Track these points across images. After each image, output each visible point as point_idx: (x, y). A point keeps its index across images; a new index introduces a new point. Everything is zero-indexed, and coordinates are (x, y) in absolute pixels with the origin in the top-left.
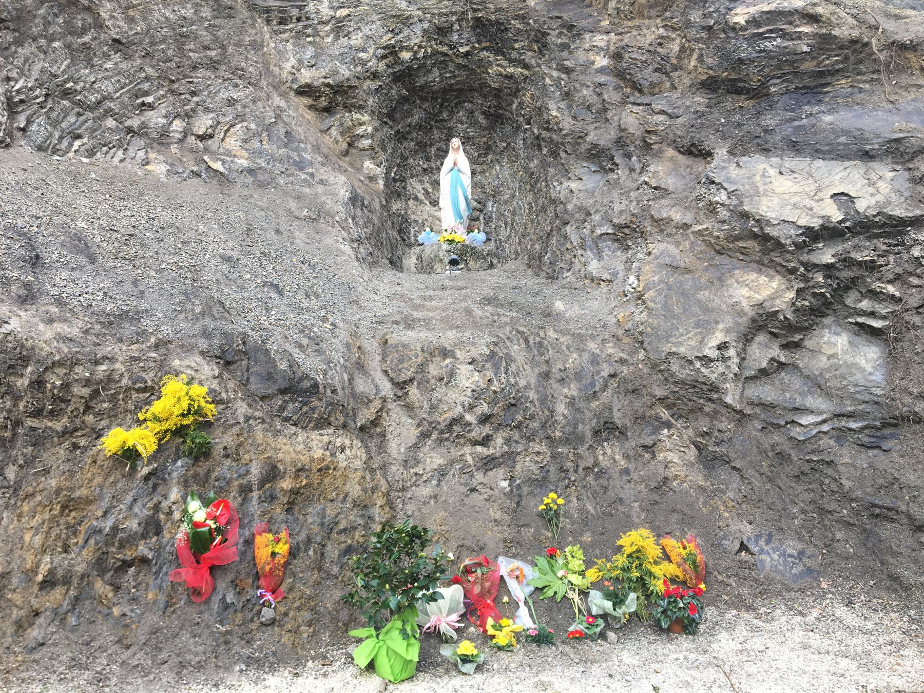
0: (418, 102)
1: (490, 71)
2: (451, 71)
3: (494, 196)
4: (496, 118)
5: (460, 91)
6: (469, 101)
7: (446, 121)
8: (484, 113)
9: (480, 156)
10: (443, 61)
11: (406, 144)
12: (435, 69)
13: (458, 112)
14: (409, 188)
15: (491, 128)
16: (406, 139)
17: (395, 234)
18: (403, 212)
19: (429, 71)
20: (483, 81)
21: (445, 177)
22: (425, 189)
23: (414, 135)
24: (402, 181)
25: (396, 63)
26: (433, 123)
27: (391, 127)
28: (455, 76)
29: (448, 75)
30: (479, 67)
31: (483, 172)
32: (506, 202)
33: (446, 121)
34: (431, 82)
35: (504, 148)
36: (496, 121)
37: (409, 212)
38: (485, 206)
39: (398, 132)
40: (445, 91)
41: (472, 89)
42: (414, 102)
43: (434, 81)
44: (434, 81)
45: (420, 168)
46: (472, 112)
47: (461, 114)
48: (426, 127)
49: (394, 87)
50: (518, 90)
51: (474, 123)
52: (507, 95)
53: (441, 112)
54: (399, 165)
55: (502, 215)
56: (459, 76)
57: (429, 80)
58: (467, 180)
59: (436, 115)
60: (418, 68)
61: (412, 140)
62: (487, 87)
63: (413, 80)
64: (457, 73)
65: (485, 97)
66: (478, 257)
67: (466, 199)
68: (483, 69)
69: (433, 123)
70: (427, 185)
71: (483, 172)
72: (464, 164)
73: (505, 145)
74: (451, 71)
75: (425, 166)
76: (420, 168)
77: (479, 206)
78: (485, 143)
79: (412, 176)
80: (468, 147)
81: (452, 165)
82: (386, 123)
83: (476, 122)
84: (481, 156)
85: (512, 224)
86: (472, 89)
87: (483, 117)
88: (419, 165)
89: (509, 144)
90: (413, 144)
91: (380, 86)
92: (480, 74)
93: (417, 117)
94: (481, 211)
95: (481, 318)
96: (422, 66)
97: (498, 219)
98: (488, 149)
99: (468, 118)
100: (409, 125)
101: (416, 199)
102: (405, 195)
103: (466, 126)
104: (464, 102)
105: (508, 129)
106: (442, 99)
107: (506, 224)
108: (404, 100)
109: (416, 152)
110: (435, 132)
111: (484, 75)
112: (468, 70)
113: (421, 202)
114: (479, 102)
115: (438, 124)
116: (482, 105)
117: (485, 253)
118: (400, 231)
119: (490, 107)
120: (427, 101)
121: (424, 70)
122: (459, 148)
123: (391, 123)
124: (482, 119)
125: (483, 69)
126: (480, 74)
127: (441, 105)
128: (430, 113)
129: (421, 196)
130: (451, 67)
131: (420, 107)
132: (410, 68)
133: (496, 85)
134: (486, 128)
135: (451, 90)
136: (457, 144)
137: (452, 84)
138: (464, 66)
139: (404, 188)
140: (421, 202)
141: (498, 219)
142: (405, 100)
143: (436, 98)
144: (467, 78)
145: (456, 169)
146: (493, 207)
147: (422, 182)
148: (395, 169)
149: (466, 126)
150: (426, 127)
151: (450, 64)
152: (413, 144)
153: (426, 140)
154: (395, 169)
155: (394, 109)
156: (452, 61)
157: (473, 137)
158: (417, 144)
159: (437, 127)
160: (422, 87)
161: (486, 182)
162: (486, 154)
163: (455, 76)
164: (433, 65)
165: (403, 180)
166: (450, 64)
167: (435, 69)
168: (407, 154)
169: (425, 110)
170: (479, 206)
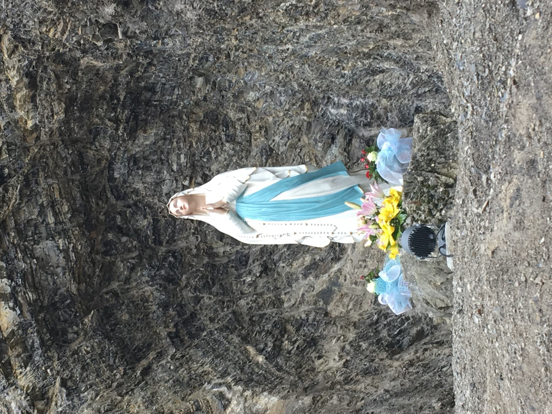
0: (115, 285)
1: (30, 124)
2: (42, 213)
3: (315, 103)
4: (140, 105)
5: (86, 189)
6: (110, 167)
7: (156, 221)
8: (132, 134)
9: (231, 139)
10: (20, 232)
11: (203, 319)
12: (39, 250)
13: (136, 192)
14: (301, 313)
15: (167, 115)
16: (193, 315)
17: (396, 365)
18: (351, 336)
19: (44, 263)
20: (56, 138)
21: (264, 232)
22: (308, 271)
23: (188, 294)
24: (284, 331)
25: (22, 342)
26: (163, 249)
27: (160, 355)
28: (53, 204)
29: (51, 219)
30: (27, 149)
31: (265, 130)
32: (323, 74)
33: (156, 221)
34: (67, 258)
35: (207, 81)
36: (148, 103)
37: (355, 316)
38: (339, 125)
39: (174, 337)
40: (88, 226)
41: (81, 162)
42: (115, 294)
43: (65, 251)
44: (65, 251)
45: (261, 282)
46: (134, 160)
47: (139, 186)
48: (172, 266)
49: (74, 346)
50: (58, 58)
51: (159, 156)
52: (76, 82)
53: (137, 232)
54: (245, 339)
55: (355, 82)
56: (50, 196)
57: (62, 262)
58: (263, 178)
59: (144, 245)
60: (35, 288)
61: (197, 300)
62: (70, 131)
63: (63, 298)
64: (43, 200)
65: (95, 133)
66: (440, 151)
67: (305, 179)
68: (31, 140)
69: (163, 249)
70: (298, 266)
71: (265, 130)
72: (221, 187)
73: (199, 81)
74: (42, 213)
75: (257, 269)
76: (261, 282)
77: (340, 139)
78: (202, 128)
79: (278, 303)
80: (214, 167)
81: (226, 216)
82: (147, 371)
83: (155, 148)
84: (225, 136)
85: (368, 56)
86: (81, 162)
87: (141, 135)
88: (253, 284)
89: (196, 72)
90: (207, 299)
91: (63, 383)
92: (43, 147)
93: (146, 288)
94: (350, 135)
95: (519, 226)
96: (30, 280)
97: (365, 91)
98: (214, 119)
99: (147, 168)
100: (165, 306)
101: (326, 295)
102: (315, 325)
103: (166, 174)
104: (111, 179)
105: (157, 75)
106: (107, 231)
107: (374, 72)
108: (107, 325)
109: (225, 291)
110: (182, 244)
111: (44, 138)
112: (35, 174)
113: (334, 282)
114: (107, 144)
115: (165, 238)
116: (113, 138)
117: (431, 132)
118: (394, 348)
119: (116, 121)
120: (113, 263)
121: (41, 276)
122: (190, 199)
123: (152, 355)
124: (146, 139)
125: (31, 140)
126: (43, 147)
127: (121, 231)
128: (140, 257)
129: (321, 283)
130: (30, 213)
131: (128, 280)
132: (36, 308)
133: (59, 108)
134: (167, 125)
135: (88, 212)
136: (181, 203)
137: (74, 211)
138: (27, 183)
139: (300, 325)
140: (334, 282)
141: (365, 91)
142: (107, 314)
143: (107, 243)
144: (55, 175)
145: (246, 205)
146: (339, 106)
147: (291, 280)
148: (251, 350)
149: (166, 174)
150: (172, 266)
151: (24, 216)
152: (207, 299)
153: (200, 265)
154: (251, 350)
155: (123, 347)
156: (17, 210)
157: (191, 156)
158: (207, 287)
159: (172, 240)
160: (79, 277)
161: (287, 124)
162: (228, 123)
163: (53, 204)
164: (28, 253)
165: (281, 327)
166: (24, 216)
167: (39, 250)
168: (225, 313)
169: (132, 269)
170: (340, 139)
